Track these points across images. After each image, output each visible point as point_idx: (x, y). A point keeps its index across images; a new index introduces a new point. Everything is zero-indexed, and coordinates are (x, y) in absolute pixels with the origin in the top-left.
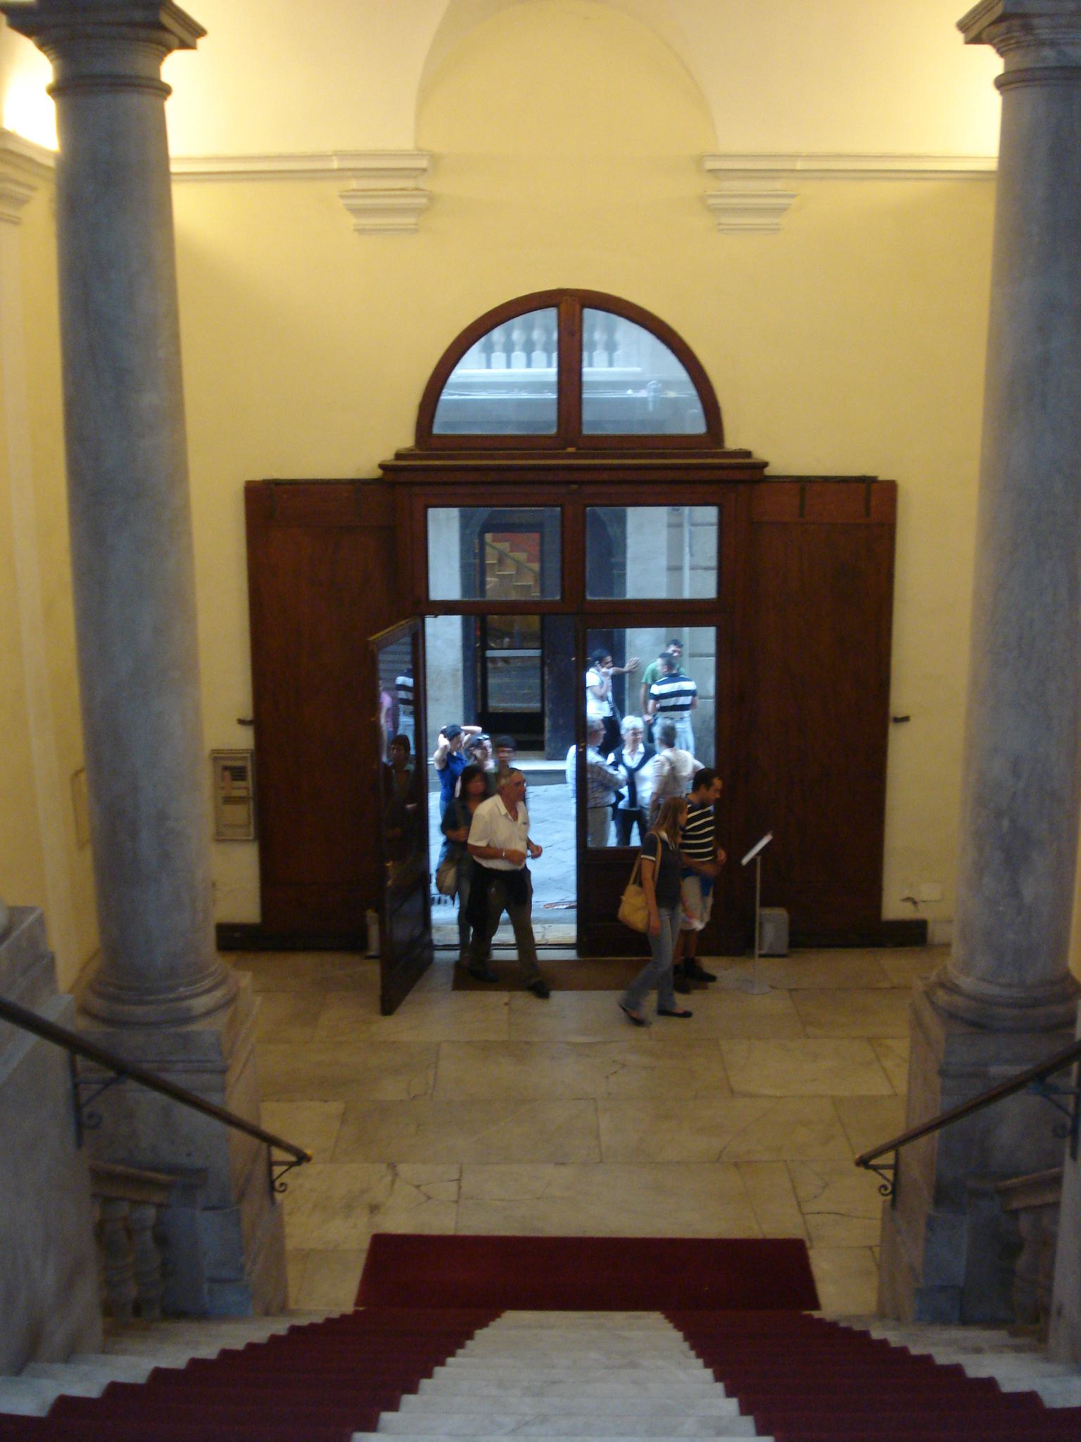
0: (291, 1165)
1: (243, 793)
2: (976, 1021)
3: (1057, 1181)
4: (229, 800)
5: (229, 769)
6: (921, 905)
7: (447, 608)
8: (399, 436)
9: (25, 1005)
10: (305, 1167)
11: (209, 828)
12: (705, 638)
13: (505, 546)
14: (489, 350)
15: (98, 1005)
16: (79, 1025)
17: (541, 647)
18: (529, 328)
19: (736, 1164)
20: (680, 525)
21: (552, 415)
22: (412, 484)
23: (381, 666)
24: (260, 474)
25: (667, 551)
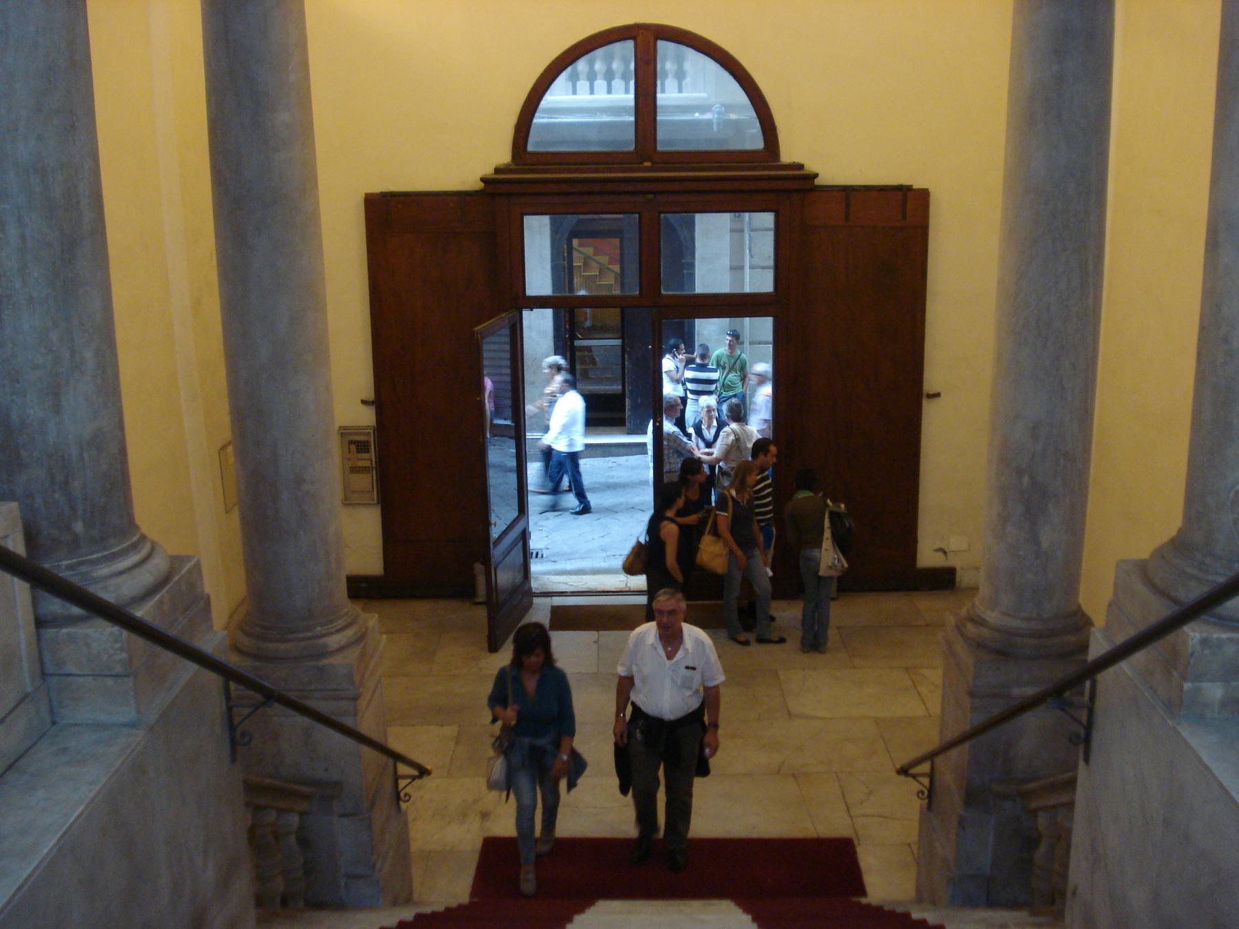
0: (414, 778)
1: (368, 464)
2: (1001, 649)
3: (1071, 784)
4: (354, 470)
5: (354, 442)
6: (950, 555)
7: (540, 302)
8: (495, 153)
9: (185, 639)
10: (426, 779)
11: (339, 496)
12: (762, 328)
13: (589, 251)
14: (574, 79)
15: (247, 642)
16: (232, 660)
17: (622, 338)
18: (609, 60)
19: (794, 776)
20: (742, 231)
21: (631, 135)
22: (510, 195)
23: (485, 355)
24: (378, 187)
25: (729, 252)
